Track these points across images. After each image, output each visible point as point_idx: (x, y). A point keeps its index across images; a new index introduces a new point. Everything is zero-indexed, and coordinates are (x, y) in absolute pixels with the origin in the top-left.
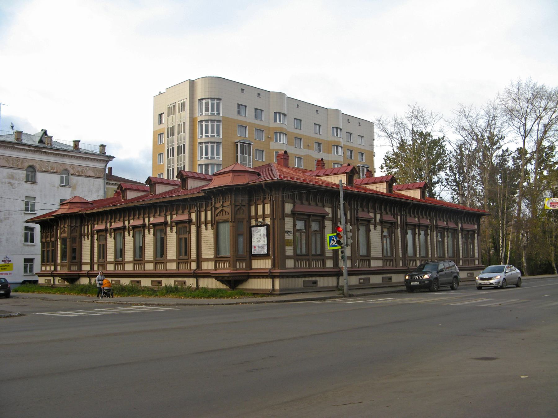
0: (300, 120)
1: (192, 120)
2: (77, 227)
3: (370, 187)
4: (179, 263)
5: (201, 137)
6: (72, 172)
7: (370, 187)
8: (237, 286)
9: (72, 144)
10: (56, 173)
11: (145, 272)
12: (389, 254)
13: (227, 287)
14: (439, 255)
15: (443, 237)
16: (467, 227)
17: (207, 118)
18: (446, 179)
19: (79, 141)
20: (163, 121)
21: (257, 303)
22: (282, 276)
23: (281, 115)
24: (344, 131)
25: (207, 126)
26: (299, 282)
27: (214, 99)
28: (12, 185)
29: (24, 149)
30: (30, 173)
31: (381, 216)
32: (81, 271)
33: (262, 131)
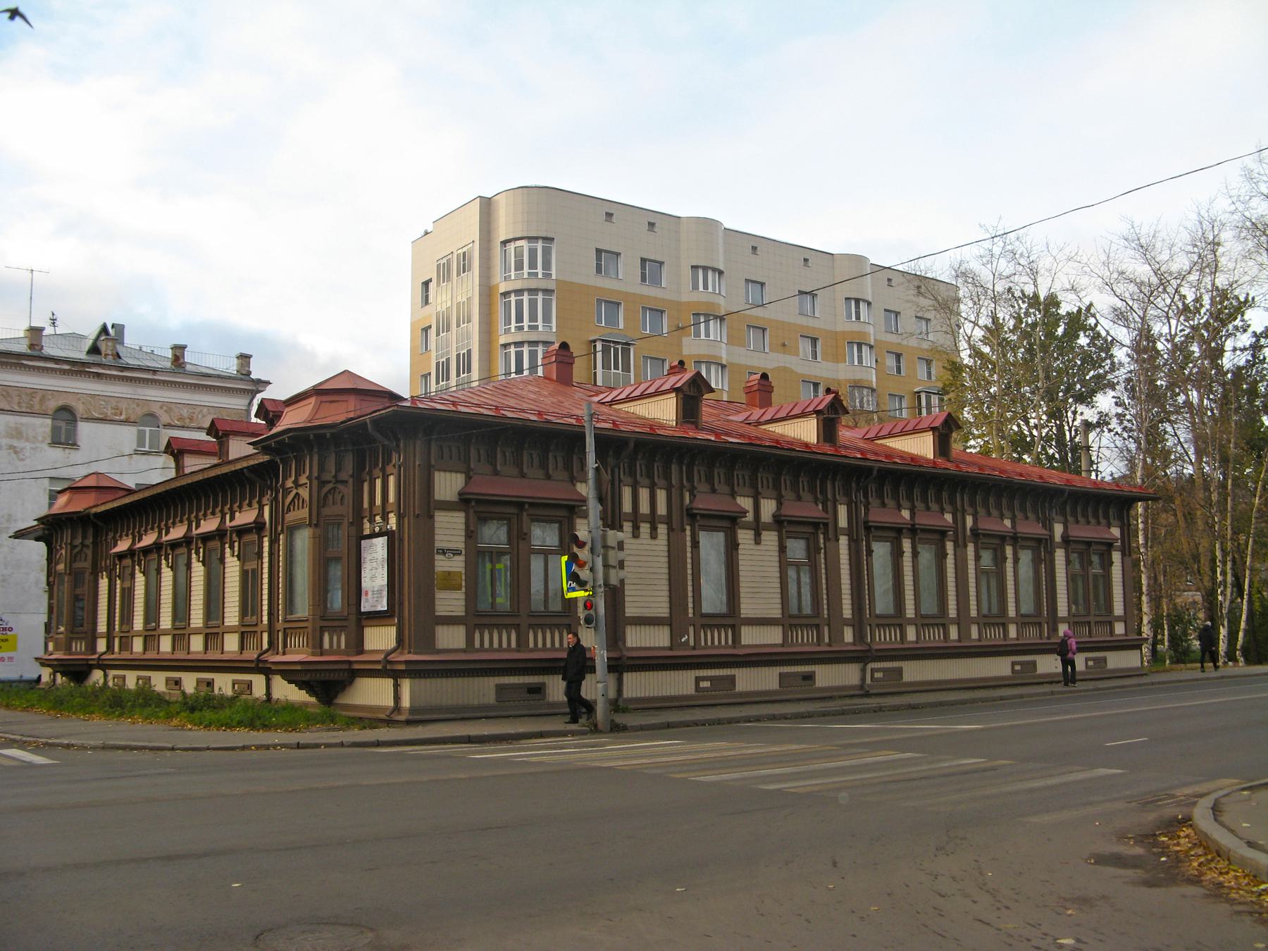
0: (762, 284)
1: (487, 292)
2: (87, 546)
3: (778, 429)
4: (243, 633)
5: (507, 331)
6: (165, 419)
7: (778, 429)
8: (336, 696)
9: (169, 354)
10: (127, 422)
11: (190, 657)
12: (807, 610)
13: (313, 700)
14: (985, 611)
15: (1000, 560)
16: (1082, 531)
17: (518, 285)
18: (1118, 416)
19: (183, 348)
20: (431, 300)
21: (299, 746)
22: (416, 671)
23: (710, 273)
24: (878, 308)
25: (519, 305)
26: (484, 689)
27: (536, 238)
28: (16, 452)
29: (111, 377)
30: (63, 424)
31: (780, 504)
32: (361, 651)
33: (662, 312)
